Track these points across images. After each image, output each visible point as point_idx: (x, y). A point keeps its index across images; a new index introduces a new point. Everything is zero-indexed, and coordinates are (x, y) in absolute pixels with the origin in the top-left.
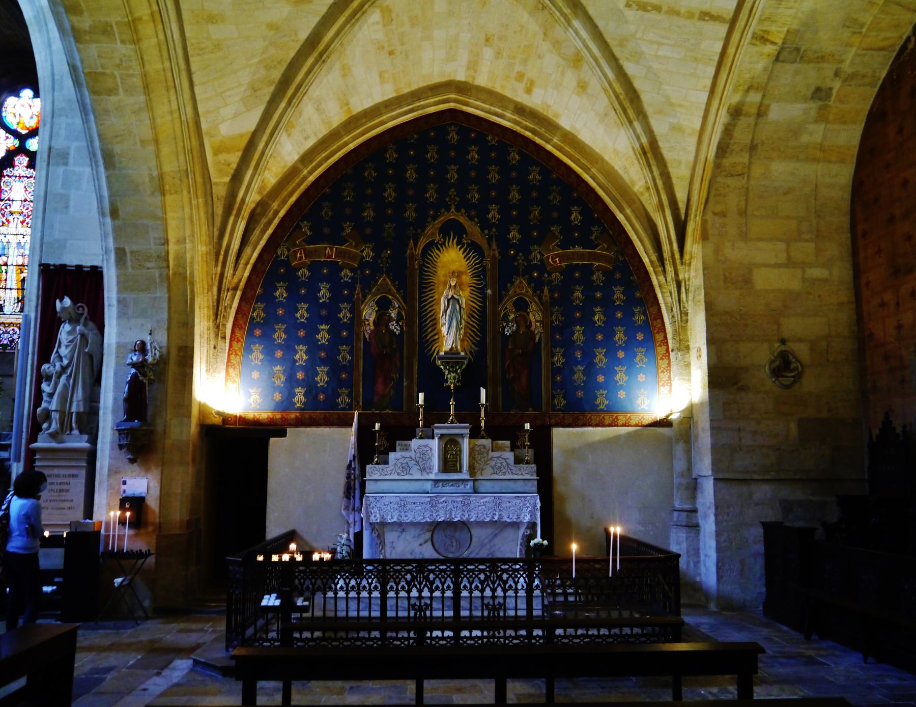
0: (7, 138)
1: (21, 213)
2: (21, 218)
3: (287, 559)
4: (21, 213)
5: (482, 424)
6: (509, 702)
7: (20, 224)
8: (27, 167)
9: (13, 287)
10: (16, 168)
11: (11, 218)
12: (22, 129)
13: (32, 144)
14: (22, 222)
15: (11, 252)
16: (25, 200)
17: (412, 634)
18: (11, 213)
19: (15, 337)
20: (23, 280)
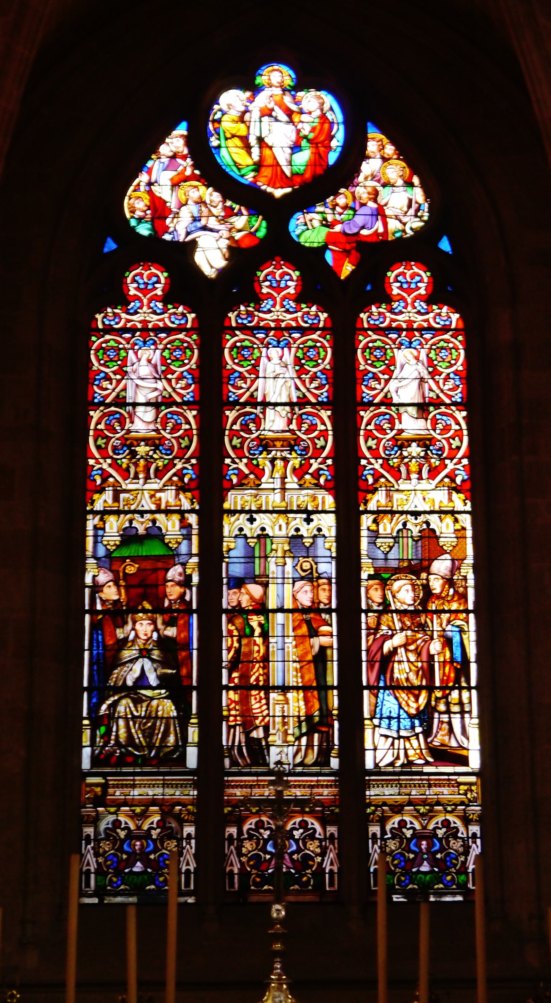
0: (229, 213)
1: (292, 444)
2: (295, 462)
3: (337, 760)
4: (292, 444)
5: (170, 671)
6: (367, 767)
7: (292, 482)
8: (299, 299)
9: (292, 681)
10: (267, 305)
11: (263, 461)
12: (272, 183)
13: (308, 229)
14: (300, 472)
15: (273, 568)
16: (303, 402)
17: (124, 608)
18: (265, 445)
19: (313, 847)
20: (320, 659)
